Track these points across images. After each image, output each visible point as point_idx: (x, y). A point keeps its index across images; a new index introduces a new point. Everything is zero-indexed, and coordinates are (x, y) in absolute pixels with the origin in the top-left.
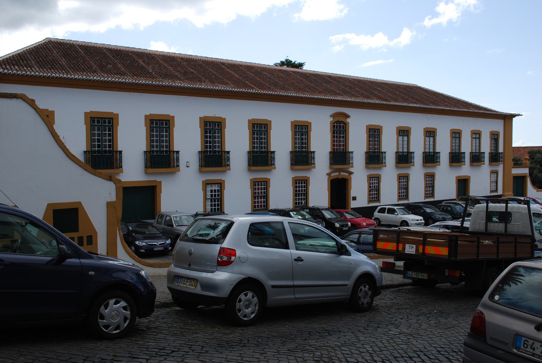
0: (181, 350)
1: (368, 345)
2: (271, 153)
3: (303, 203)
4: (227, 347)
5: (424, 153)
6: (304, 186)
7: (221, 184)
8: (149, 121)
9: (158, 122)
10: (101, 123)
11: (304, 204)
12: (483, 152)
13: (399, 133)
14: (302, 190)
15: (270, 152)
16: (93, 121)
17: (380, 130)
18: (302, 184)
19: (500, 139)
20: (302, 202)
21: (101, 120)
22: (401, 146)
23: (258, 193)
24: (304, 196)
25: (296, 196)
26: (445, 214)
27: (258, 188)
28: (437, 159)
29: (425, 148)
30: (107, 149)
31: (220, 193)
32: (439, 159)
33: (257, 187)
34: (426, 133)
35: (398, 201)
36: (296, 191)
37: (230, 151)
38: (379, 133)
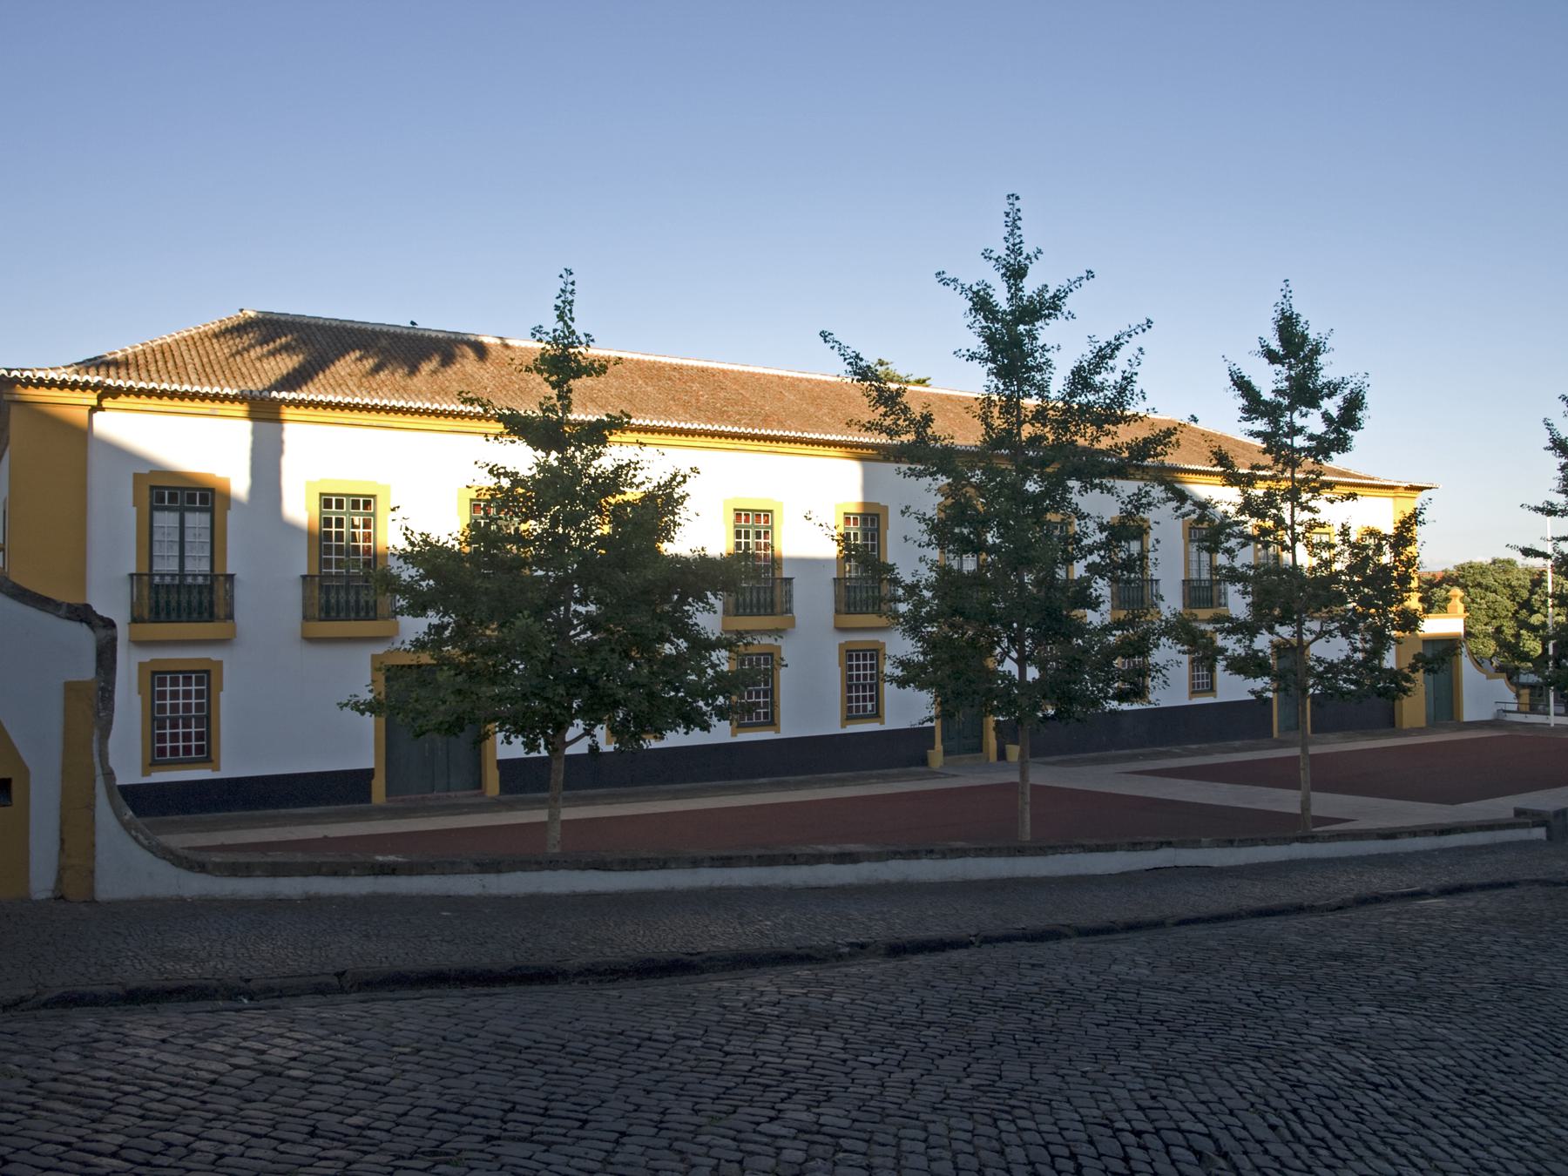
0: (749, 1080)
1: (1013, 1125)
2: (226, 580)
3: (869, 708)
4: (478, 1159)
5: (1186, 582)
6: (872, 665)
7: (206, 677)
8: (147, 493)
9: (179, 492)
10: (182, 501)
11: (873, 710)
12: (786, 579)
13: (1190, 536)
14: (865, 676)
15: (221, 578)
16: (738, 516)
17: (881, 517)
18: (865, 658)
19: (889, 532)
20: (865, 708)
21: (347, 501)
22: (1194, 566)
23: (858, 676)
24: (871, 690)
25: (850, 691)
26: (809, 776)
27: (865, 669)
28: (1220, 597)
29: (1187, 570)
30: (334, 570)
31: (204, 701)
32: (157, 602)
33: (854, 663)
34: (1190, 532)
35: (1190, 699)
36: (851, 677)
37: (792, 579)
38: (878, 525)
